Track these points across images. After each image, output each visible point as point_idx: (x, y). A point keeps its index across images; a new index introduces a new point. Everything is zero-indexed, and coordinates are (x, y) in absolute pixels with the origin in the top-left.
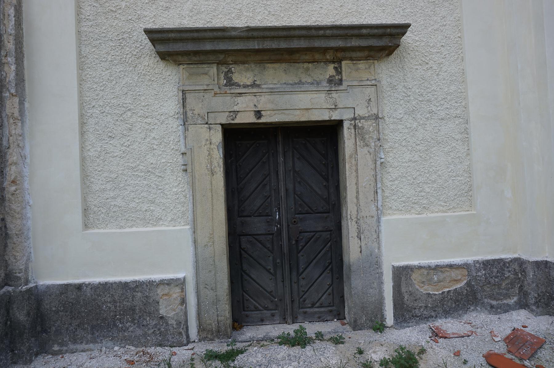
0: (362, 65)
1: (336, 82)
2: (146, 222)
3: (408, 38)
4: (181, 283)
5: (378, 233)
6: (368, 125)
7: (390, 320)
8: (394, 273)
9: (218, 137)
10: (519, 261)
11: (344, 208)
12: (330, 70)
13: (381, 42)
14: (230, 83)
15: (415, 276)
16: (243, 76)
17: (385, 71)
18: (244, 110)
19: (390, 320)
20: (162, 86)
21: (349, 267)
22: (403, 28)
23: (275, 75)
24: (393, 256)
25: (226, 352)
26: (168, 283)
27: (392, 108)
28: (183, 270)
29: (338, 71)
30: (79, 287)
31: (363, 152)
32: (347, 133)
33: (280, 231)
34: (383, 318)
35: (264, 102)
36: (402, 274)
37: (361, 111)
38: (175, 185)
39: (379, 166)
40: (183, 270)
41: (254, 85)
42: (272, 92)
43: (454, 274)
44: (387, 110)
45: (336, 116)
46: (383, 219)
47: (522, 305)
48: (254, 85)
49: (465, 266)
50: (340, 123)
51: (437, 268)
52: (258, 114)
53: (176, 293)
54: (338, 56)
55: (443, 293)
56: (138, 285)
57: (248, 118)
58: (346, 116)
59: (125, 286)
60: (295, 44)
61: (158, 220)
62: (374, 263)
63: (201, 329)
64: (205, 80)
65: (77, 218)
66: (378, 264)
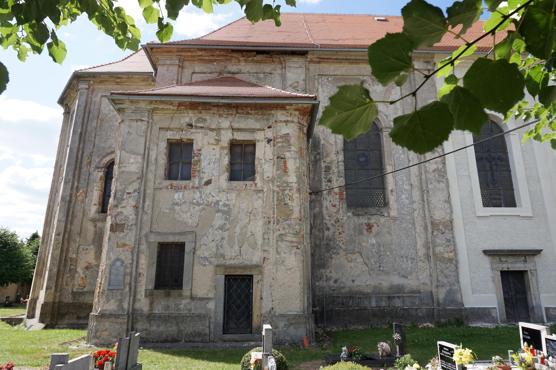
0: (531, 257)
1: (525, 261)
2: (485, 293)
3: (294, 7)
4: (495, 308)
5: (540, 298)
6: (534, 272)
7: (546, 321)
9: (499, 273)
11: (529, 293)
12: (523, 258)
13: (537, 252)
14: (501, 261)
16: (503, 259)
17: (536, 259)
18: (505, 267)
19: (546, 321)
20: (486, 261)
22: (542, 250)
23: (510, 259)
27: (539, 268)
28: (496, 306)
29: (525, 258)
30: (474, 308)
31: (533, 278)
32: (529, 273)
33: (512, 298)
34: (544, 320)
36: (547, 309)
37: (532, 268)
38: (491, 285)
39: (537, 282)
41: (506, 261)
42: (511, 263)
44: (537, 268)
45: (526, 269)
46: (541, 295)
48: (506, 261)
52: (508, 268)
53: (495, 311)
55: (525, 340)
56: (487, 308)
58: (528, 269)
59: (484, 308)
60: (517, 253)
62: (540, 306)
63: (501, 321)
64: (496, 260)
66: (540, 306)
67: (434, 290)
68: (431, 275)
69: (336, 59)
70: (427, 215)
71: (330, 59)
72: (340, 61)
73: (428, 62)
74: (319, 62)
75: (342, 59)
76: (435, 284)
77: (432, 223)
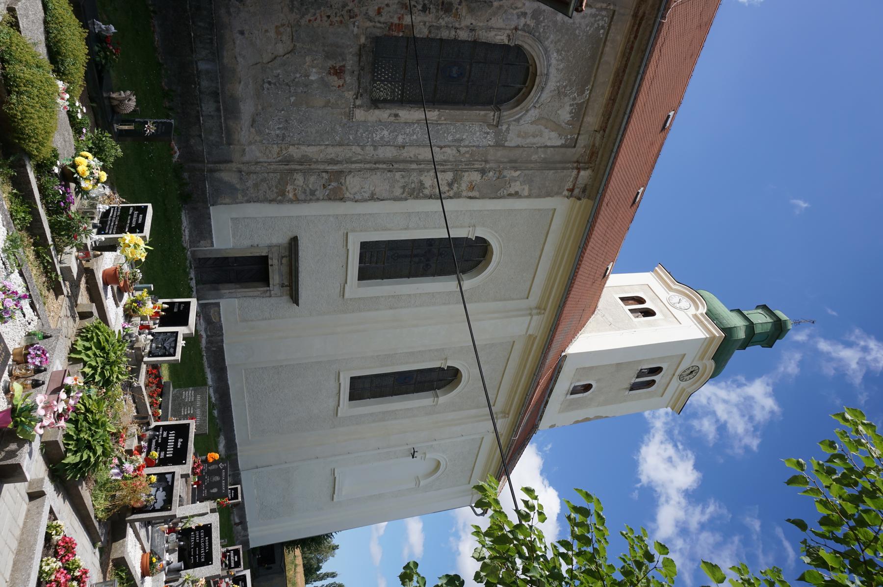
4: (212, 245)
6: (268, 294)
7: (200, 302)
8: (212, 561)
9: (264, 254)
10: (222, 334)
14: (283, 257)
15: (216, 309)
16: (284, 261)
18: (274, 262)
19: (200, 302)
21: (218, 289)
22: (298, 305)
23: (285, 269)
24: (223, 303)
25: (87, 55)
26: (212, 243)
28: (216, 246)
30: (210, 218)
35: (276, 267)
36: (218, 305)
38: (247, 243)
39: (254, 297)
40: (216, 246)
41: (282, 264)
43: (218, 319)
47: (207, 336)
49: (220, 320)
50: (269, 286)
51: (219, 314)
54: (290, 286)
57: (270, 262)
61: (234, 237)
65: (234, 215)
66: (220, 298)
67: (234, 166)
68: (257, 163)
69: (632, 48)
70: (353, 166)
71: (636, 37)
72: (626, 55)
73: (584, 190)
74: (635, 15)
75: (628, 59)
76: (244, 168)
77: (341, 172)
